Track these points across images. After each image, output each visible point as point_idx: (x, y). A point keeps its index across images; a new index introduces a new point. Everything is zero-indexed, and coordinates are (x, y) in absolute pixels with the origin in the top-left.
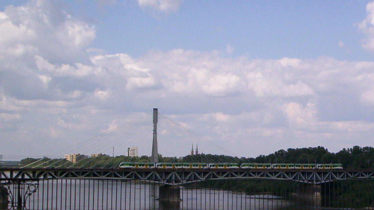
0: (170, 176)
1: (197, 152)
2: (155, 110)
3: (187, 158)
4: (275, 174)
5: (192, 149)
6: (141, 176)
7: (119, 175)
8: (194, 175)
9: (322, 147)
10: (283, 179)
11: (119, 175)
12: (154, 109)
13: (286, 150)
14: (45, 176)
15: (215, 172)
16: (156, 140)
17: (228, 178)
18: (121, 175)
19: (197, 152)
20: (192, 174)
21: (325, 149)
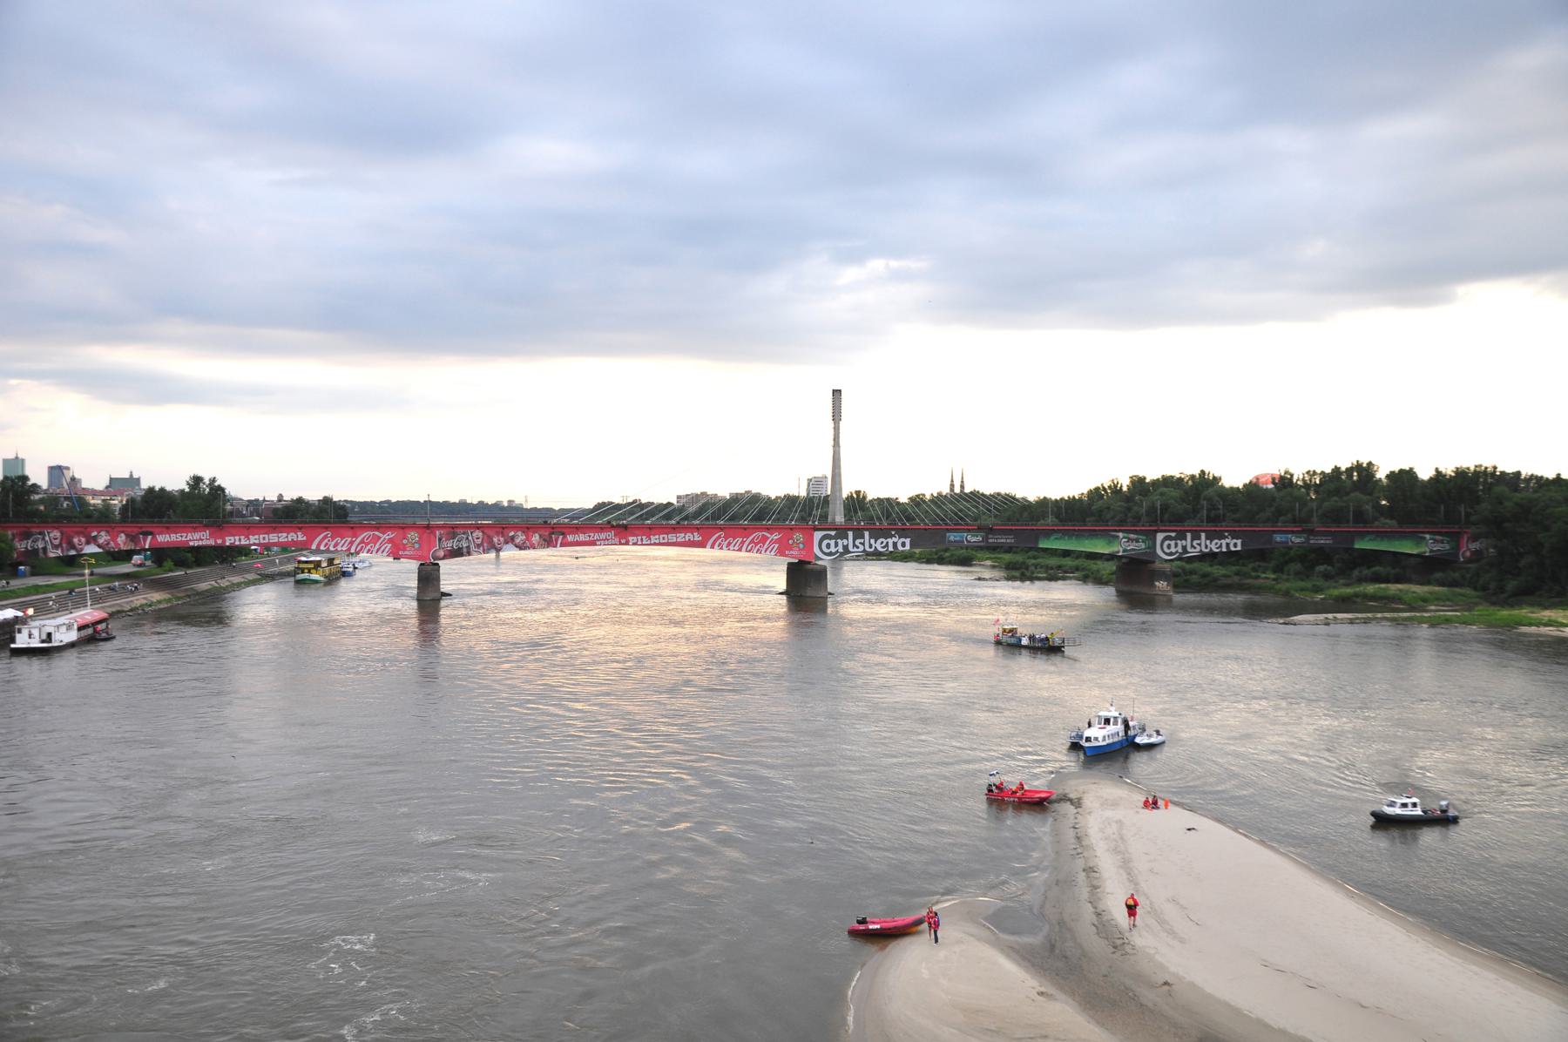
1: (962, 487)
2: (837, 393)
19: (962, 487)
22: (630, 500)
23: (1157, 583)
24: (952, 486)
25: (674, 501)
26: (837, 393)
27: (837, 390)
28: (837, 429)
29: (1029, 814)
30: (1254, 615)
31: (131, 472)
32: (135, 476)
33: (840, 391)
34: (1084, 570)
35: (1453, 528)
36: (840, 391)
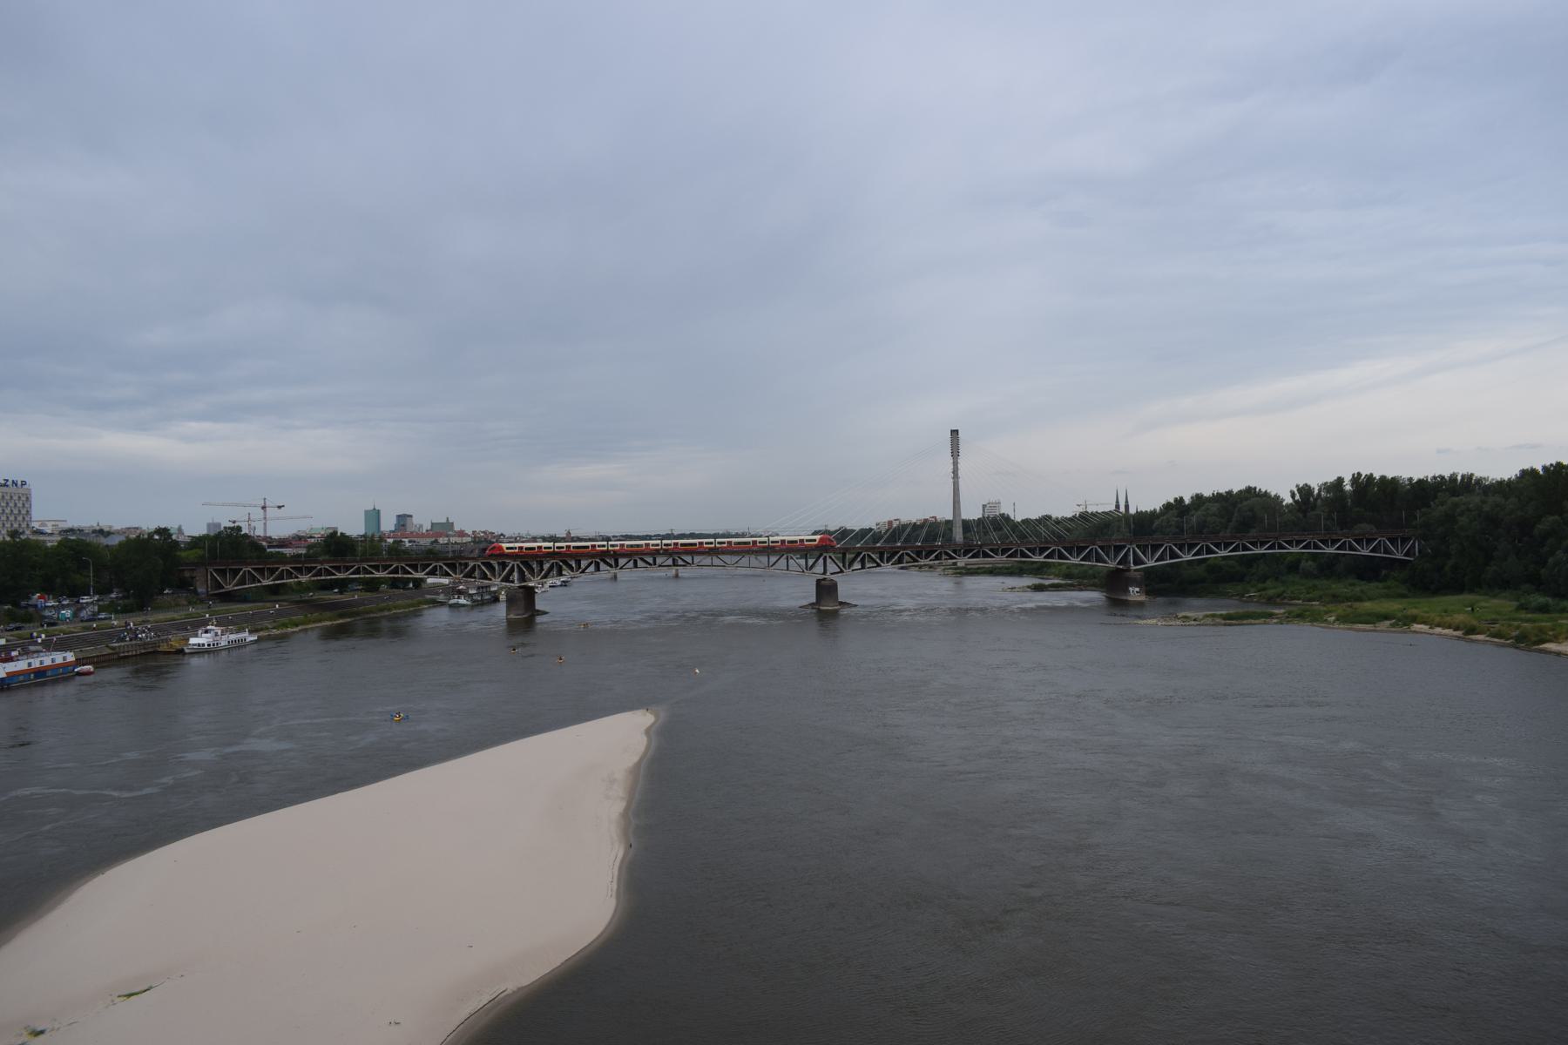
0: (1159, 554)
1: (1127, 507)
2: (955, 433)
3: (438, 573)
4: (1189, 550)
5: (1117, 502)
6: (1108, 556)
7: (1030, 554)
8: (1171, 549)
9: (1266, 491)
10: (1384, 555)
11: (1030, 554)
12: (952, 431)
13: (1172, 501)
14: (863, 561)
15: (912, 551)
16: (959, 502)
17: (977, 559)
18: (996, 554)
19: (1127, 507)
20: (1129, 549)
21: (1273, 494)
22: (838, 528)
23: (1131, 589)
24: (1118, 506)
25: (874, 527)
26: (955, 433)
27: (954, 431)
28: (955, 464)
29: (625, 814)
30: (514, 635)
31: (448, 519)
32: (451, 521)
33: (957, 431)
34: (1078, 580)
35: (632, 546)
36: (957, 431)
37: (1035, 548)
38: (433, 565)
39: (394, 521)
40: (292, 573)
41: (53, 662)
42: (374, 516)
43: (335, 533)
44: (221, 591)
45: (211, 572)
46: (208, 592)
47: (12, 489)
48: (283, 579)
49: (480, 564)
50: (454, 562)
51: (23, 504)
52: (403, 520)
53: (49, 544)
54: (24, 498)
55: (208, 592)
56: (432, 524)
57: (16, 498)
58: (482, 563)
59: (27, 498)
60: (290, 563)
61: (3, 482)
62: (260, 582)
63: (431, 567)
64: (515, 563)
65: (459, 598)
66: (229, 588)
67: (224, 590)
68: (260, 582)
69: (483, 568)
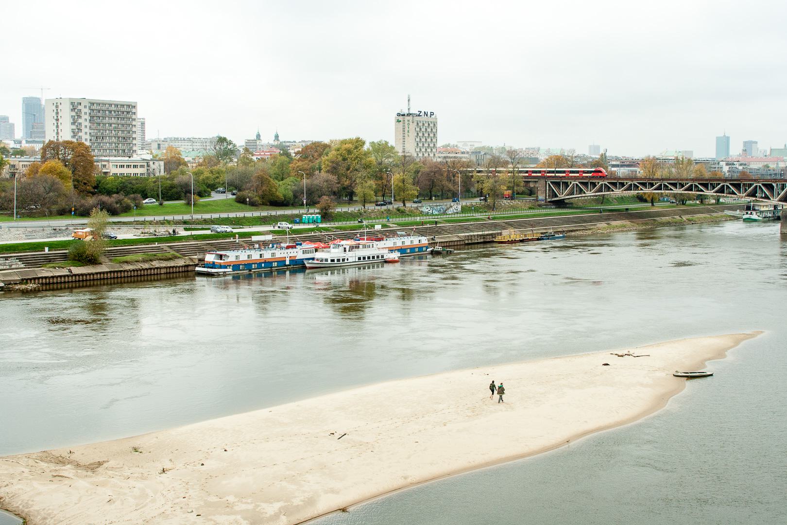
37: (646, 183)
38: (721, 184)
39: (741, 147)
40: (638, 187)
41: (248, 257)
42: (724, 142)
43: (359, 138)
44: (556, 199)
45: (549, 184)
46: (546, 199)
47: (424, 118)
48: (602, 192)
49: (761, 185)
50: (740, 182)
51: (426, 129)
52: (748, 146)
53: (464, 160)
54: (432, 125)
55: (546, 199)
56: (771, 149)
57: (421, 124)
58: (763, 184)
59: (434, 125)
60: (608, 179)
61: (418, 113)
62: (584, 193)
63: (719, 186)
64: (758, 184)
65: (751, 214)
66: (561, 197)
67: (557, 199)
68: (584, 193)
69: (763, 188)
